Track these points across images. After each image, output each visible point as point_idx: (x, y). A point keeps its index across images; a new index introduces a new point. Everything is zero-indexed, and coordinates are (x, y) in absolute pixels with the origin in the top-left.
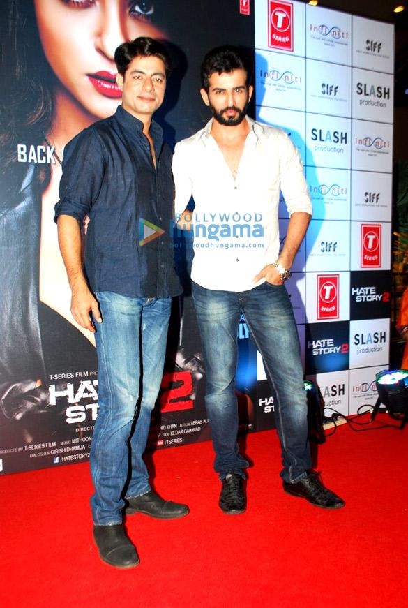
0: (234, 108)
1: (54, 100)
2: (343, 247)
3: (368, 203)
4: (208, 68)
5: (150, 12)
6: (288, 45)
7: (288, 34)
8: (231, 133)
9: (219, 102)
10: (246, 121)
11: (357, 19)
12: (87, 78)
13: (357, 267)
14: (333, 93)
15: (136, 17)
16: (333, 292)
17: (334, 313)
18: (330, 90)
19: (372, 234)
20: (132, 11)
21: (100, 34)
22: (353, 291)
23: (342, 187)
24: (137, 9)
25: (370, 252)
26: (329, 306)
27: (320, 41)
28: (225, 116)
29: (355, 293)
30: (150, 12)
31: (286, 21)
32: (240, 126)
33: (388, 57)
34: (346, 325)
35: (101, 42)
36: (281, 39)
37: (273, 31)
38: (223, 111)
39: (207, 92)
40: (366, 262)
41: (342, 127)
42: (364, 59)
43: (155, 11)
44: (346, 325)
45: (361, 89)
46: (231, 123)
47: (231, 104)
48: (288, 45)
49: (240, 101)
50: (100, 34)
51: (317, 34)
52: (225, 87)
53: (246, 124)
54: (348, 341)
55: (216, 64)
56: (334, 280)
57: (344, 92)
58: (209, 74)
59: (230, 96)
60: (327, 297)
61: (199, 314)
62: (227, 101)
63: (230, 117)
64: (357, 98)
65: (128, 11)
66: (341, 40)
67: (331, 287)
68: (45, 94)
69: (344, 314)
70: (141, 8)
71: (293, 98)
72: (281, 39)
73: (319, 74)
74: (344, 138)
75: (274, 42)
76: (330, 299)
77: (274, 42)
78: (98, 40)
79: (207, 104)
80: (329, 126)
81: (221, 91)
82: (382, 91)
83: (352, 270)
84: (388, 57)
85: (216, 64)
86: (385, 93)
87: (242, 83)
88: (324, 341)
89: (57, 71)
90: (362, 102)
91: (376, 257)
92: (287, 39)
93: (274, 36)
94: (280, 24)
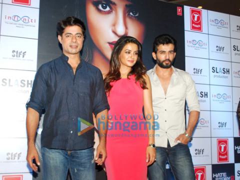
0: (169, 60)
1: (92, 54)
2: (229, 125)
3: (198, 155)
4: (158, 43)
5: (137, 15)
6: (200, 29)
7: (200, 24)
8: (164, 72)
9: (162, 57)
10: (172, 69)
11: (231, 16)
12: (108, 44)
13: (216, 162)
14: (222, 50)
15: (131, 18)
16: (225, 148)
17: (226, 159)
18: (220, 49)
19: (201, 172)
20: (129, 15)
21: (114, 25)
22: (214, 175)
23: (228, 95)
24: (131, 14)
25: (223, 154)
26: (223, 155)
27: (215, 27)
28: (164, 64)
29: (215, 177)
30: (137, 15)
31: (198, 18)
32: (169, 69)
33: (228, 54)
34: (232, 166)
35: (115, 28)
36: (196, 26)
37: (193, 22)
38: (164, 61)
39: (156, 53)
40: (220, 159)
41: (227, 66)
42: (215, 55)
43: (139, 15)
44: (232, 166)
45: (214, 70)
46: (167, 67)
47: (168, 58)
48: (200, 29)
49: (171, 57)
50: (114, 25)
51: (213, 23)
52: (165, 51)
53: (172, 69)
54: (234, 174)
55: (161, 41)
56: (226, 142)
57: (228, 49)
58: (158, 45)
59: (167, 54)
60: (222, 150)
61: (169, 145)
62: (166, 57)
63: (167, 64)
64: (234, 52)
65: (127, 14)
66: (225, 26)
67: (201, 174)
68: (89, 52)
69: (231, 160)
70: (133, 13)
71: (203, 53)
72: (196, 26)
73: (215, 42)
74: (228, 71)
75: (193, 28)
76: (224, 151)
77: (193, 28)
78: (113, 28)
79: (155, 59)
80: (220, 66)
81: (163, 52)
82: (203, 94)
83: (213, 163)
84: (228, 54)
85: (161, 41)
86: (205, 95)
87: (173, 50)
88: (221, 174)
89: (94, 41)
90: (215, 76)
91: (226, 156)
92: (199, 26)
93: (193, 25)
94: (196, 19)
